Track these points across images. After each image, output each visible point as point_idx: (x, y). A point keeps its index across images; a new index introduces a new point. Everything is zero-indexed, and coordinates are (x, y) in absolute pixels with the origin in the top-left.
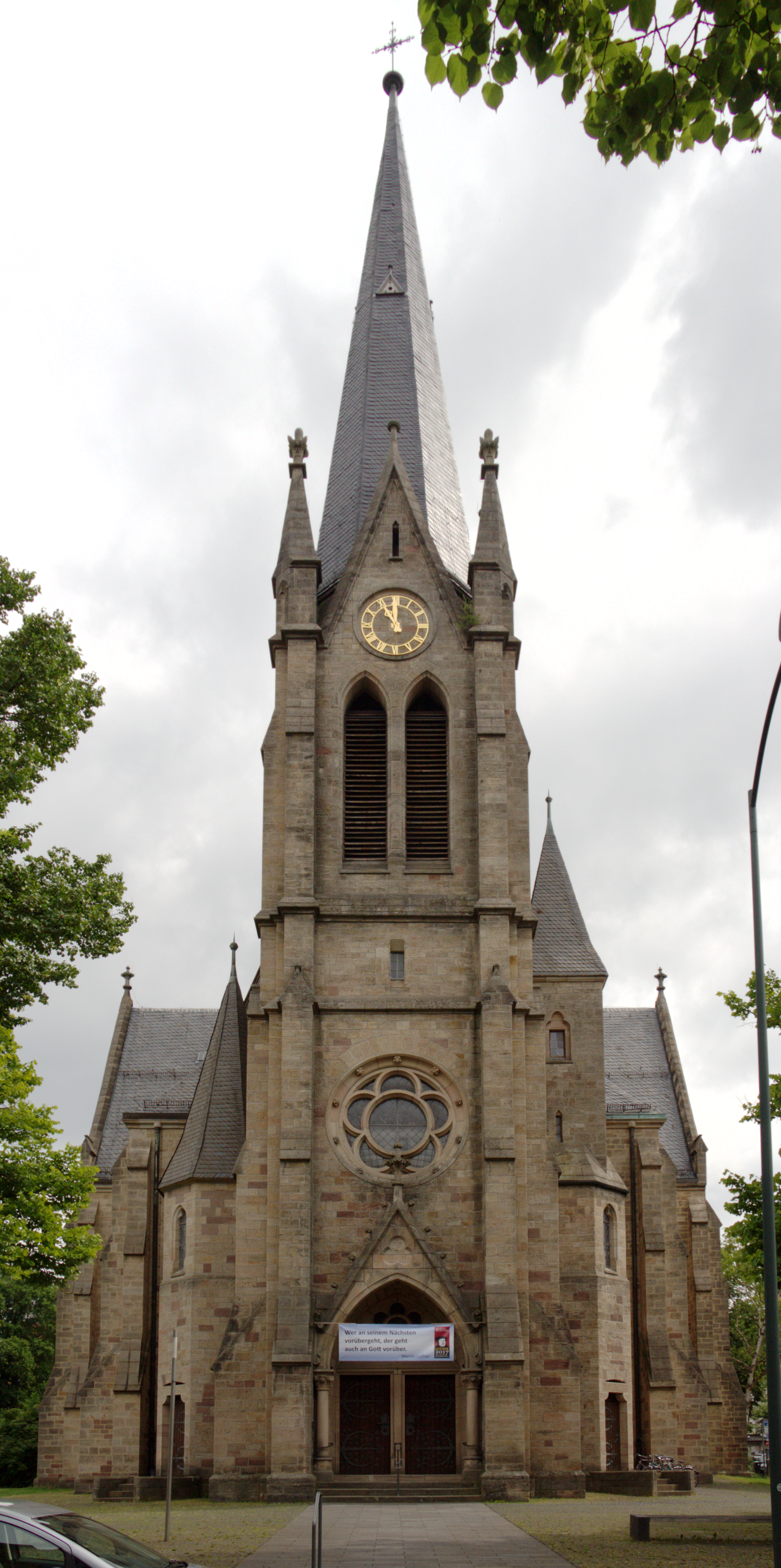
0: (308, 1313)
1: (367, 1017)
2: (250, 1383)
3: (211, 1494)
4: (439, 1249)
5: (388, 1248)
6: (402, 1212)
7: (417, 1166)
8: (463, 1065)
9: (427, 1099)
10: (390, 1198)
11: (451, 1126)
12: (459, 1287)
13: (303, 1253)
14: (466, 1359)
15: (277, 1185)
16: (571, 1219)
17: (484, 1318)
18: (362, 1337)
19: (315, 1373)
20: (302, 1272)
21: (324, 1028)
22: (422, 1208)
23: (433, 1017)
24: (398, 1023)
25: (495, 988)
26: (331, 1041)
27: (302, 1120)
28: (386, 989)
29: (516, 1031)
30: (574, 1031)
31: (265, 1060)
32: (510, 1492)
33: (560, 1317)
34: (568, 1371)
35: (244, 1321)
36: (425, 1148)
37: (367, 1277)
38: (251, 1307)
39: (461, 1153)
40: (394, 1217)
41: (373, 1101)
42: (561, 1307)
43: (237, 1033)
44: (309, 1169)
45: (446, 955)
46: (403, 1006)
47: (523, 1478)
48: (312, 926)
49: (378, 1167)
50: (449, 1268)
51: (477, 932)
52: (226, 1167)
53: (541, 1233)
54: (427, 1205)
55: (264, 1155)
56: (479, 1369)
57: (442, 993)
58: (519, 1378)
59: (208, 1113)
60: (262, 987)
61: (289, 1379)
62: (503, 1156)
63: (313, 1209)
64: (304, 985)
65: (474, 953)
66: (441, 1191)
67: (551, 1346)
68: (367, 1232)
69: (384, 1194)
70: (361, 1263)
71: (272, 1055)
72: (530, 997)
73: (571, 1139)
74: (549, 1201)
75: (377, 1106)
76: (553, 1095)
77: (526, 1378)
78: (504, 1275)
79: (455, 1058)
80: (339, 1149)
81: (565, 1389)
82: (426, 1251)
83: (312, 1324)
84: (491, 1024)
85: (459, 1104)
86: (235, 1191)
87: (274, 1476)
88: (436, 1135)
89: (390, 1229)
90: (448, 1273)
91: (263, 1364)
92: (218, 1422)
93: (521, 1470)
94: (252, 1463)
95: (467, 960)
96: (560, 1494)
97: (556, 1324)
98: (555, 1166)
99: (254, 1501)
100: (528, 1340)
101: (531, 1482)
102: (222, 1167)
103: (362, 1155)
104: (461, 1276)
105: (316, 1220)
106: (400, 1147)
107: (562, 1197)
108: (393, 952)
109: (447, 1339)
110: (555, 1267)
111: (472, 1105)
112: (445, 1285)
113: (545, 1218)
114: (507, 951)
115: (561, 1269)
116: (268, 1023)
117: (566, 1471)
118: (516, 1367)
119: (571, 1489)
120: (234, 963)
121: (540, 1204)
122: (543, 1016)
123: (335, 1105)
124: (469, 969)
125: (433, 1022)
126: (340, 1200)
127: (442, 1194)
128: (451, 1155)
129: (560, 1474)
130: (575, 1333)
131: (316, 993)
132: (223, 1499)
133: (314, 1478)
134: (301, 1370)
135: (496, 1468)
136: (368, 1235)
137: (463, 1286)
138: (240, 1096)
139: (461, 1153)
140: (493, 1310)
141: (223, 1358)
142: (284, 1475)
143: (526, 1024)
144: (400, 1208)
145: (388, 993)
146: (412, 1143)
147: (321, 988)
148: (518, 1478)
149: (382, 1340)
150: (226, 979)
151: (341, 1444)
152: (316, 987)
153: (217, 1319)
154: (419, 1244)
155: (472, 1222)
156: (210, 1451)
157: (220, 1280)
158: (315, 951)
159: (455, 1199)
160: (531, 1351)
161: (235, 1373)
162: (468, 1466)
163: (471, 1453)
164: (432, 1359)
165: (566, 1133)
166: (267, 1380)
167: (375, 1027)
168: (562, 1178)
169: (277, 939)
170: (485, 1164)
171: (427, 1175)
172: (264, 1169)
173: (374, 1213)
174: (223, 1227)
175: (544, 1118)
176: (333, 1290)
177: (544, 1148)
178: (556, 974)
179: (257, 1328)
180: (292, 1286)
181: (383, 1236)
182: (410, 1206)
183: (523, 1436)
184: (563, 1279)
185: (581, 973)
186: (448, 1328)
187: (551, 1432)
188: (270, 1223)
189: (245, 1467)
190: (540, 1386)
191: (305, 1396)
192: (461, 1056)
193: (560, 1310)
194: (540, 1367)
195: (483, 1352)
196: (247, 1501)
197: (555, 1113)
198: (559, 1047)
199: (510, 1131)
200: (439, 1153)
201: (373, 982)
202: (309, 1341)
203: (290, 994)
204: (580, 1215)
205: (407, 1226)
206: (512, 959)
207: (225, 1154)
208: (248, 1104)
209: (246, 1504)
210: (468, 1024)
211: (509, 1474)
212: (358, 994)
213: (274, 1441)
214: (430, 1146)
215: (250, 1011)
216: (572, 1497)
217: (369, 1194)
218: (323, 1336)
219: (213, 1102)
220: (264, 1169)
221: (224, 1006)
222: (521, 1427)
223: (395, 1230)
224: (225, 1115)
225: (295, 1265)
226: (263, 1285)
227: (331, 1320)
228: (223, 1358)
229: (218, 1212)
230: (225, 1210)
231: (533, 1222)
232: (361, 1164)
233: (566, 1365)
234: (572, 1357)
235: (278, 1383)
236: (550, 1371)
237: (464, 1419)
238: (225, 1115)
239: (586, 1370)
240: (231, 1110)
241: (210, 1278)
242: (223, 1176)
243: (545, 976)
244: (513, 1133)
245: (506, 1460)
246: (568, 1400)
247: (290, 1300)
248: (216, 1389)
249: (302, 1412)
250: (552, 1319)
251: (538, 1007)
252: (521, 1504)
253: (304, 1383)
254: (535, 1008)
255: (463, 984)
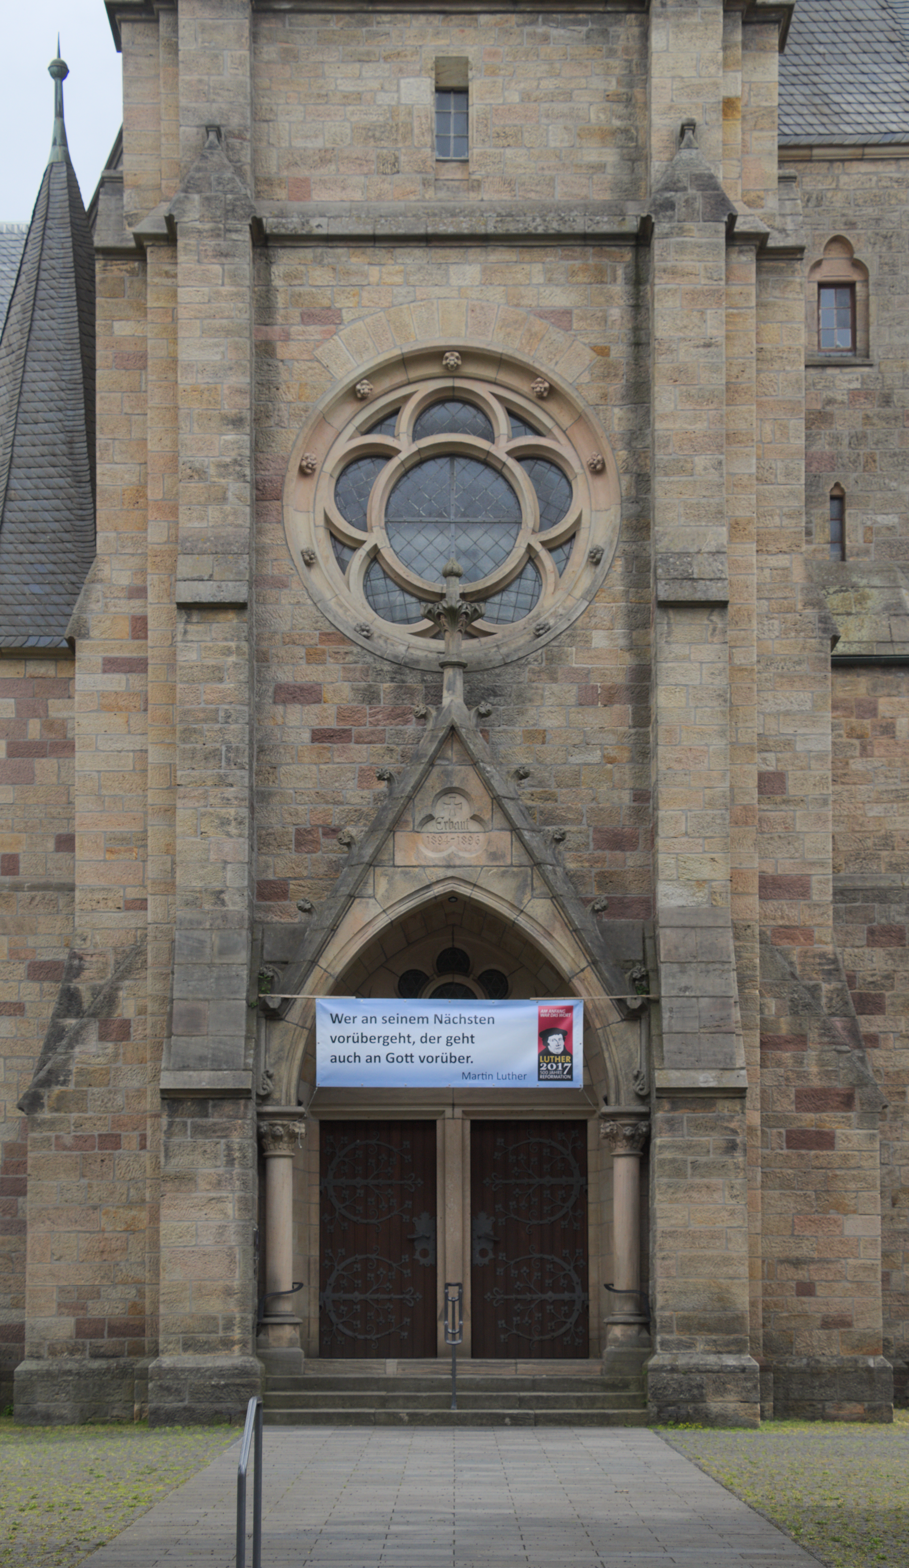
0: (244, 973)
1: (380, 254)
2: (111, 1141)
3: (18, 1407)
4: (549, 818)
5: (430, 818)
6: (463, 731)
7: (498, 620)
8: (608, 373)
9: (522, 455)
10: (435, 695)
11: (578, 521)
12: (596, 912)
13: (233, 829)
14: (612, 1083)
15: (171, 665)
16: (864, 749)
17: (653, 985)
18: (370, 1030)
19: (261, 1115)
20: (229, 874)
21: (277, 282)
22: (511, 722)
23: (537, 253)
24: (453, 269)
25: (685, 182)
26: (295, 313)
27: (228, 508)
28: (425, 183)
29: (734, 289)
30: (879, 285)
31: (139, 361)
32: (714, 1405)
33: (834, 985)
34: (852, 1114)
35: (95, 991)
36: (518, 575)
37: (382, 885)
38: (111, 958)
39: (601, 589)
40: (443, 741)
41: (395, 462)
42: (835, 961)
43: (73, 291)
44: (245, 627)
45: (568, 96)
46: (465, 227)
47: (743, 1370)
48: (247, 23)
49: (408, 621)
50: (571, 866)
51: (645, 36)
52: (51, 620)
53: (790, 783)
54: (521, 713)
55: (139, 592)
56: (642, 1109)
57: (560, 195)
58: (734, 1132)
59: (7, 489)
60: (128, 179)
61: (199, 1130)
62: (699, 596)
63: (254, 724)
64: (228, 175)
65: (638, 92)
66: (554, 680)
67: (811, 1055)
68: (380, 778)
69: (421, 687)
70: (369, 852)
71: (156, 349)
72: (771, 203)
73: (867, 552)
74: (808, 706)
75: (405, 474)
76: (822, 446)
77: (751, 1130)
78: (701, 883)
79: (588, 356)
80: (315, 577)
81: (845, 1158)
82: (519, 822)
83: (253, 999)
84: (674, 272)
85: (598, 470)
86: (72, 678)
87: (166, 1361)
88: (544, 543)
89: (436, 771)
90: (570, 877)
91: (140, 1094)
92: (35, 1233)
93: (740, 1352)
94: (114, 1331)
95: (620, 109)
96: (832, 1412)
97: (824, 1001)
98: (824, 620)
99: (119, 1421)
100: (757, 1041)
101: (763, 1382)
102: (40, 621)
103: (369, 592)
104: (600, 886)
105: (261, 750)
106: (458, 575)
107: (841, 695)
108: (441, 91)
109: (567, 1035)
110: (822, 864)
111: (627, 471)
112: (563, 907)
113: (799, 747)
114: (715, 84)
115: (836, 869)
116: (145, 271)
117: (846, 1355)
118: (728, 1103)
119: (859, 1401)
120: (60, 113)
121: (787, 713)
122: (800, 250)
123: (305, 472)
124: (625, 131)
125: (538, 267)
126: (318, 701)
127: (555, 687)
128: (578, 593)
129: (833, 1363)
130: (868, 1024)
131: (258, 195)
132: (47, 1419)
133: (257, 1364)
134: (228, 1108)
135: (681, 1345)
136: (383, 786)
137: (604, 908)
138: (81, 447)
139: (601, 589)
140: (676, 967)
141: (46, 1082)
142: (189, 1360)
143: (759, 271)
144: (458, 722)
145: (430, 193)
146: (486, 564)
147: (269, 182)
148: (733, 1371)
149: (415, 1038)
150: (44, 155)
151: (323, 1287)
152: (257, 180)
153: (35, 986)
154: (501, 807)
155: (626, 754)
156: (18, 1304)
157: (39, 894)
158: (255, 87)
159: (587, 699)
160: (763, 1066)
161: (74, 1116)
162: (616, 1340)
163: (623, 1309)
164: (533, 1083)
165: (855, 539)
166: (149, 1132)
167: (398, 279)
168: (841, 648)
169: (163, 55)
170: (657, 614)
171: (521, 641)
172: (139, 627)
173: (399, 733)
174: (45, 767)
175: (798, 503)
176: (302, 916)
177: (798, 575)
178: (837, 140)
179: (127, 1008)
180: (207, 907)
181: (418, 787)
182: (481, 715)
183: (744, 1270)
184: (840, 894)
185: (898, 138)
186: (569, 1009)
187: (812, 1261)
188: (154, 756)
189: (100, 1342)
190: (785, 1151)
191: (237, 1170)
192: (602, 351)
193: (832, 967)
194: (786, 1105)
195: (651, 1069)
196: (104, 1423)
197: (827, 490)
198: (841, 324)
199: (718, 535)
200: (551, 588)
201: (394, 166)
202: (248, 1038)
203: (196, 197)
204: (884, 740)
205: (475, 764)
206: (728, 105)
207: (48, 589)
208: (99, 470)
209: (101, 1429)
210: (620, 272)
211: (712, 1360)
212: (358, 196)
213: (166, 1279)
214: (530, 571)
215: (102, 238)
216: (863, 1420)
217: (386, 686)
218: (282, 1025)
219: (17, 461)
220: (139, 627)
221: (39, 224)
222: (739, 1248)
223: (447, 774)
224: (48, 493)
225: (213, 857)
226: (141, 905)
227: (298, 989)
228: (46, 1082)
229: (34, 730)
230: (49, 725)
231: (771, 756)
232: (368, 616)
233: (847, 1102)
234: (862, 1081)
235: (176, 1140)
236: (811, 1116)
237: (607, 1227)
238: (48, 493)
239: (896, 1114)
240: (62, 482)
241: (17, 888)
242: (44, 642)
243: (810, 147)
244: (724, 539)
245: (704, 1327)
246: (852, 1186)
247: (201, 942)
248: (32, 1156)
249: (231, 1209)
250: (814, 990)
251: (790, 226)
252: (741, 1432)
253: (236, 1140)
254: (783, 231)
255: (610, 170)
